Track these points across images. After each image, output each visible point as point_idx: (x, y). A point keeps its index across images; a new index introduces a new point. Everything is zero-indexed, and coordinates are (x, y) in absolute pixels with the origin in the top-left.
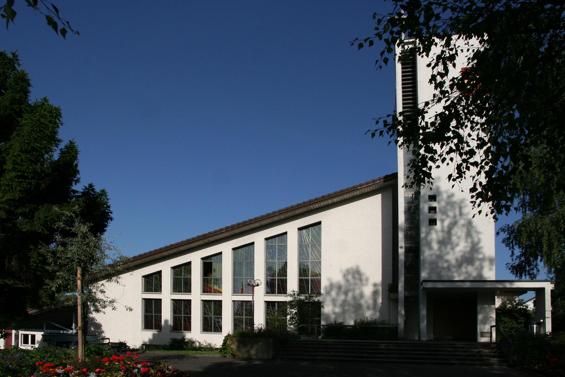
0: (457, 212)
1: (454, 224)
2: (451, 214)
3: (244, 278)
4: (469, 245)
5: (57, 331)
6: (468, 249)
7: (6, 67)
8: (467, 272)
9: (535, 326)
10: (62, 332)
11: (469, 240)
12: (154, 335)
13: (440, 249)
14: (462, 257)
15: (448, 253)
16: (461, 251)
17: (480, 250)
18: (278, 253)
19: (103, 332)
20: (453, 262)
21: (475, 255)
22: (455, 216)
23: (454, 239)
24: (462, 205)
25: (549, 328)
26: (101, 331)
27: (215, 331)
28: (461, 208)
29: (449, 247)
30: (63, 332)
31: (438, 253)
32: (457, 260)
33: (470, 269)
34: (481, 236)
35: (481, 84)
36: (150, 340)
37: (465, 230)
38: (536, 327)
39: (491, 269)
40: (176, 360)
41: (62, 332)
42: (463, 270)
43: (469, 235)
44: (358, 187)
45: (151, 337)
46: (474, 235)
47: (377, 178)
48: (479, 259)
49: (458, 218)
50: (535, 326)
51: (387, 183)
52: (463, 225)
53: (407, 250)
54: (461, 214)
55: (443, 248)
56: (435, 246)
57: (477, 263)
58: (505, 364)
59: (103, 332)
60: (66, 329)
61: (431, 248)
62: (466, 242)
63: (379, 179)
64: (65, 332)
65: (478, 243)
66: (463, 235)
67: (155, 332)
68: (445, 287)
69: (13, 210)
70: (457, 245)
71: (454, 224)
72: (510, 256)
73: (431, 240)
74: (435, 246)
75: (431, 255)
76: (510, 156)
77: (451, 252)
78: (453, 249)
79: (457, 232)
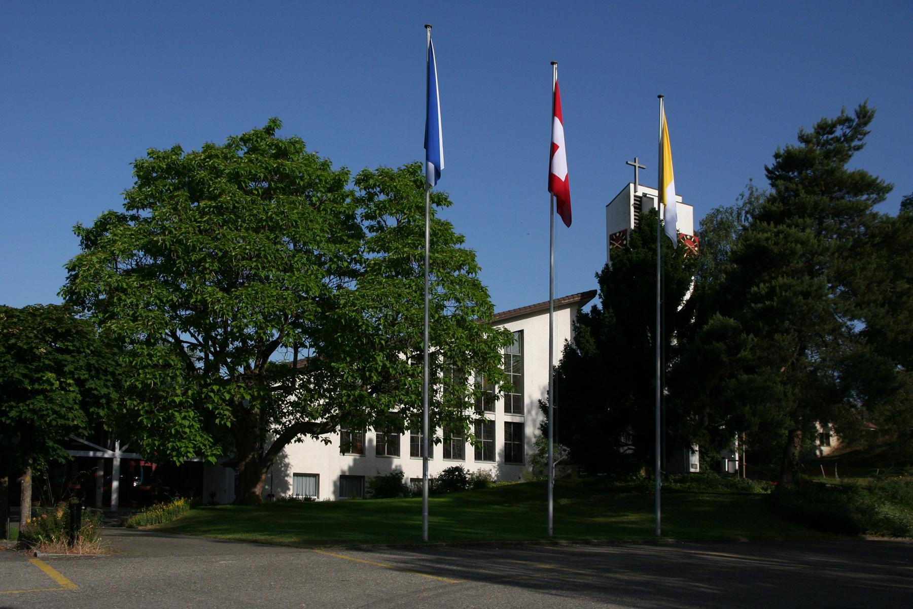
3: (483, 440)
5: (81, 453)
7: (231, 249)
10: (91, 454)
12: (355, 460)
19: (286, 456)
26: (283, 454)
27: (484, 460)
30: (94, 454)
35: (605, 474)
36: (350, 468)
40: (111, 537)
41: (91, 454)
45: (351, 464)
59: (286, 456)
60: (100, 448)
64: (99, 454)
67: (357, 456)
69: (152, 262)
76: (192, 316)
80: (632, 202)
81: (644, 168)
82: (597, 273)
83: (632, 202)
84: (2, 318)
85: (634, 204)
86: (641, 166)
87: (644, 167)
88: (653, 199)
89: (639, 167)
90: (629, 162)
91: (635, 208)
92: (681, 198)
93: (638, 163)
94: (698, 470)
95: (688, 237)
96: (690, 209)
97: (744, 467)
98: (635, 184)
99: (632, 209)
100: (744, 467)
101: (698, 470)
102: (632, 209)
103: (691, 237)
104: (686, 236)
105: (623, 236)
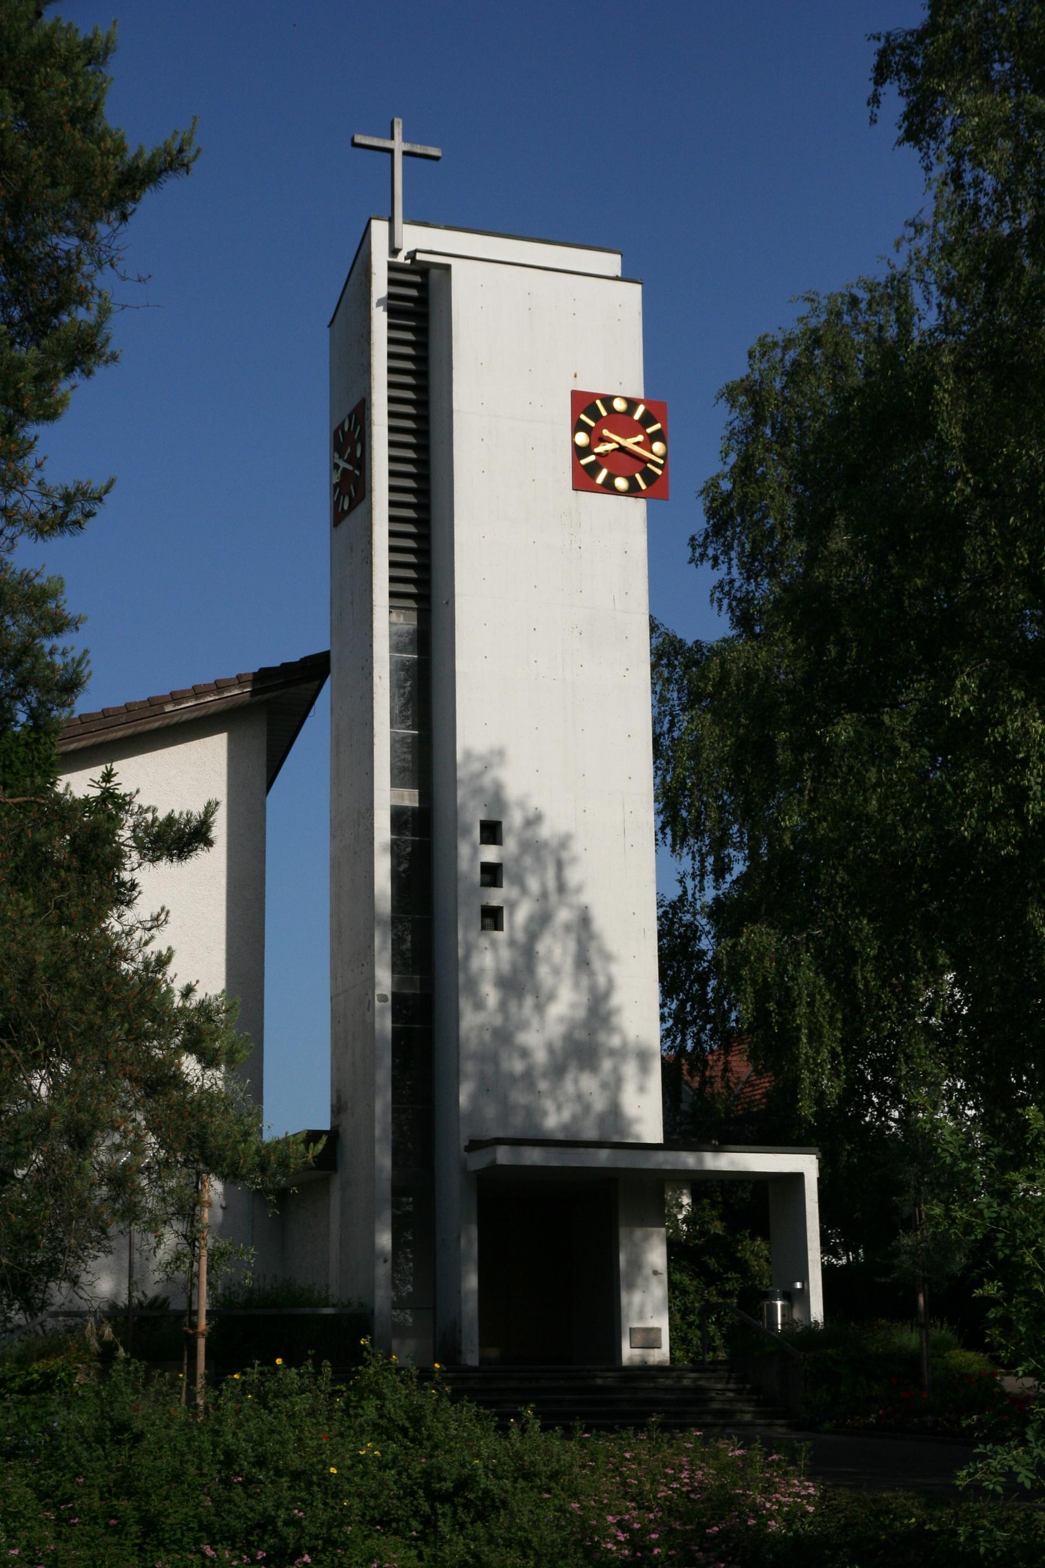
0: (551, 884)
1: (541, 921)
2: (533, 884)
4: (584, 998)
6: (581, 1013)
8: (579, 1097)
9: (779, 1303)
11: (585, 982)
13: (503, 1006)
14: (568, 1038)
15: (524, 1025)
16: (561, 1019)
17: (615, 1020)
18: (826, 1248)
20: (541, 1057)
21: (602, 1037)
22: (544, 895)
23: (543, 971)
24: (565, 855)
25: (817, 1310)
28: (560, 866)
29: (529, 1002)
31: (498, 1021)
32: (550, 1049)
33: (589, 1083)
34: (615, 969)
37: (572, 946)
38: (783, 1306)
39: (642, 1089)
42: (569, 1086)
43: (583, 963)
44: (167, 703)
46: (597, 964)
47: (231, 674)
48: (612, 1053)
49: (553, 898)
50: (779, 1303)
51: (258, 698)
52: (568, 928)
53: (399, 1002)
54: (562, 888)
55: (513, 1007)
56: (491, 995)
57: (607, 1065)
58: (782, 1422)
61: (479, 1005)
62: (576, 985)
63: (240, 681)
65: (607, 995)
66: (568, 965)
68: (554, 1163)
70: (552, 997)
71: (541, 921)
72: (77, 629)
73: (482, 970)
74: (491, 995)
75: (482, 1027)
77: (535, 1022)
78: (540, 1008)
79: (550, 952)
80: (380, 287)
81: (436, 158)
82: (713, 567)
83: (380, 287)
84: (1043, 1022)
85: (391, 296)
86: (418, 149)
87: (434, 152)
88: (447, 268)
89: (406, 153)
90: (360, 139)
91: (392, 312)
92: (617, 259)
93: (405, 139)
94: (661, 1354)
95: (619, 405)
96: (637, 289)
97: (201, 1343)
98: (391, 220)
99: (380, 319)
100: (201, 1343)
101: (661, 1354)
102: (380, 319)
103: (632, 404)
104: (608, 400)
105: (594, 414)
